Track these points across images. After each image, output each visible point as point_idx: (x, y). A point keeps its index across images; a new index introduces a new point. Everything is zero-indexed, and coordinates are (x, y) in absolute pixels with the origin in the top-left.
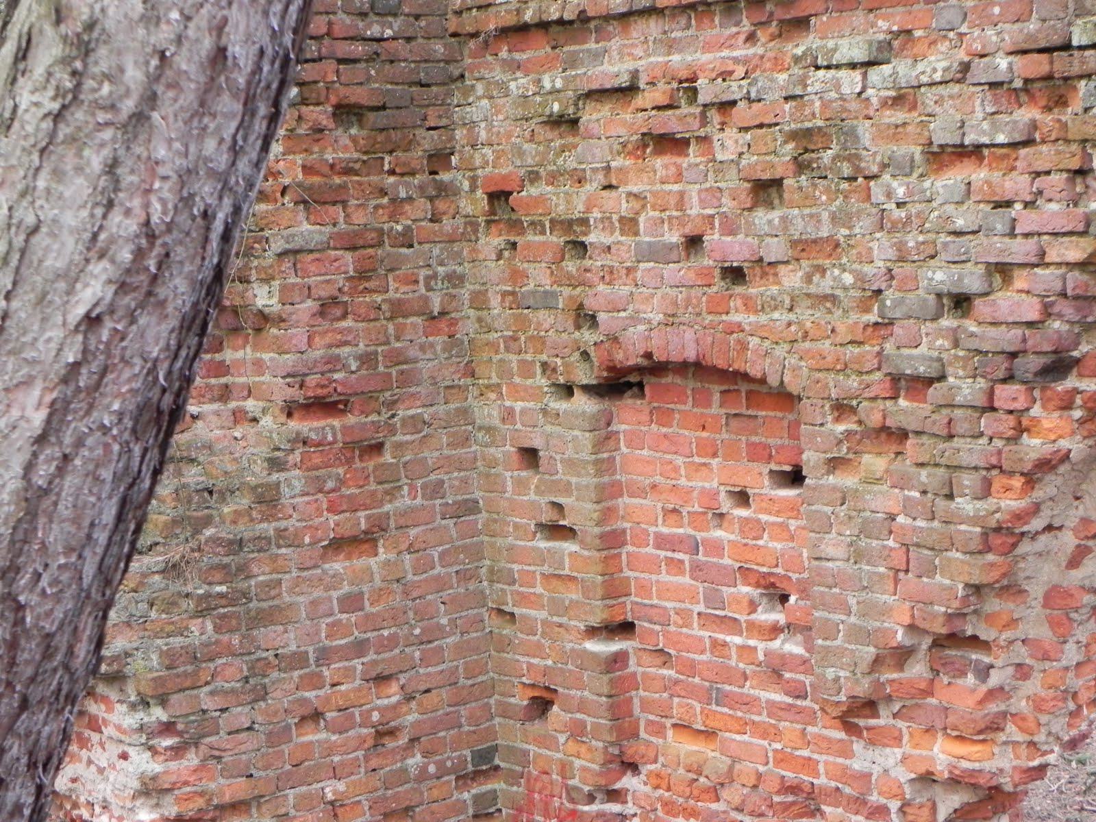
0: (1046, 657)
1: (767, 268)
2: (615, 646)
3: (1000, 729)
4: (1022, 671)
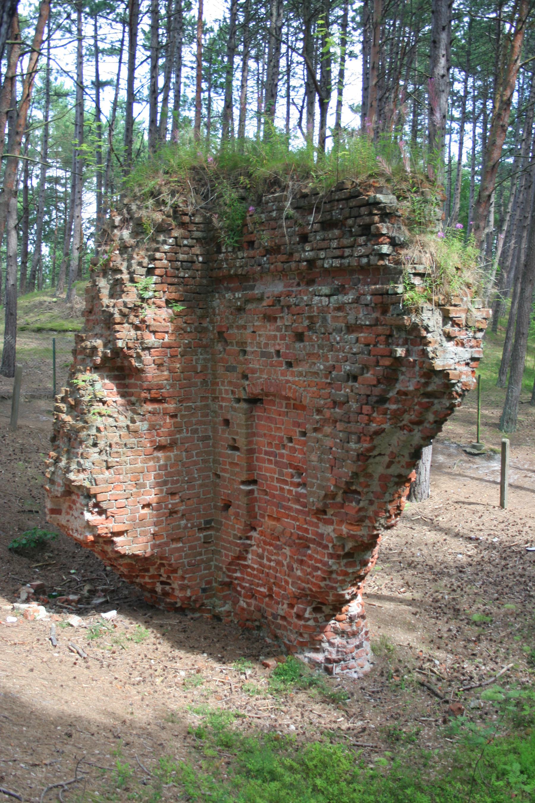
0: (378, 498)
1: (298, 361)
2: (250, 488)
3: (363, 521)
4: (371, 503)
